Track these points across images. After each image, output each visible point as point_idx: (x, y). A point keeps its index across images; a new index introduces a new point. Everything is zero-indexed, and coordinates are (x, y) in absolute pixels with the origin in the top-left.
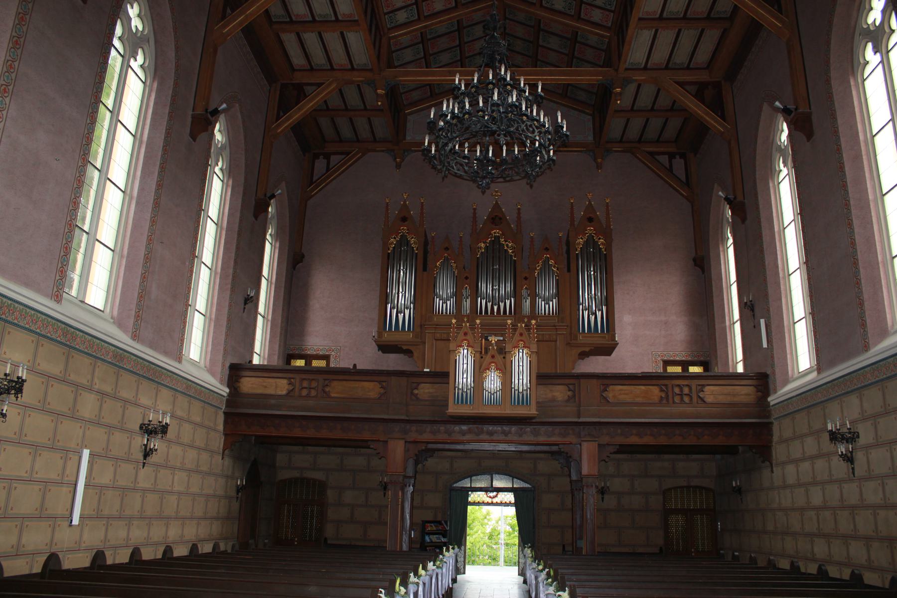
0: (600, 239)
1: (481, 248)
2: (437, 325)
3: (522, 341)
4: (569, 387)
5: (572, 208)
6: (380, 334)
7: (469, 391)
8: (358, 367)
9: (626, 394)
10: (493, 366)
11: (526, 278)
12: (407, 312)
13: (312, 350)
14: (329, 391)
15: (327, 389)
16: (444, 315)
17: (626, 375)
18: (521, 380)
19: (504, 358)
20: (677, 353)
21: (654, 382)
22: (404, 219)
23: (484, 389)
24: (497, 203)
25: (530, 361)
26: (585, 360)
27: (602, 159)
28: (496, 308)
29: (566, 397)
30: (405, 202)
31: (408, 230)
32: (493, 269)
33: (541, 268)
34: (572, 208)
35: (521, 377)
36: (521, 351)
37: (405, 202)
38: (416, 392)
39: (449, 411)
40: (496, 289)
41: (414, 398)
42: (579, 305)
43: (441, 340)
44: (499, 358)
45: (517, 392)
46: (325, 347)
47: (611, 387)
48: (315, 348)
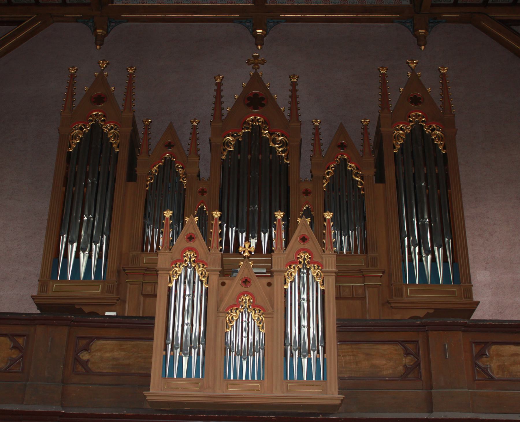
0: (433, 130)
1: (228, 144)
2: (146, 270)
6: (43, 286)
11: (307, 193)
18: (306, 329)
22: (99, 100)
25: (323, 292)
27: (426, 30)
31: (104, 116)
32: (248, 211)
35: (304, 323)
38: (85, 356)
41: (80, 369)
44: (259, 285)
47: (494, 347)
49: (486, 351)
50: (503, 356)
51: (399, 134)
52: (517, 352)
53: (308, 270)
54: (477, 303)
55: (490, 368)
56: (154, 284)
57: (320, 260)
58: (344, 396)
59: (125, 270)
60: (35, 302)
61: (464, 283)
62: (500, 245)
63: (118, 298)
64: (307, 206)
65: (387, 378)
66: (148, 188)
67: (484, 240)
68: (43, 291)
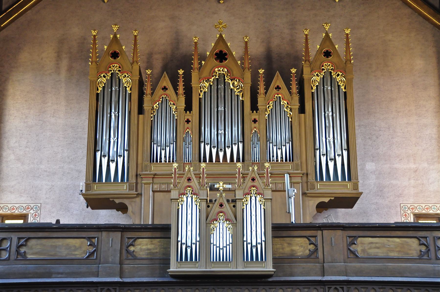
3: (221, 212)
4: (309, 240)
5: (307, 39)
6: (88, 187)
7: (194, 247)
8: (61, 222)
9: (378, 248)
10: (221, 217)
12: (120, 160)
13: (6, 209)
14: (25, 252)
15: (22, 250)
16: (163, 164)
17: (377, 225)
19: (234, 206)
20: (430, 205)
21: (410, 233)
23: (211, 243)
24: (221, 36)
26: (322, 213)
28: (221, 154)
29: (307, 252)
30: (115, 36)
33: (272, 109)
34: (307, 39)
36: (253, 198)
37: (115, 36)
38: (132, 249)
39: (171, 270)
40: (221, 134)
42: (315, 149)
43: (160, 191)
45: (249, 246)
46: (22, 205)
47: (359, 239)
48: (10, 206)
49: (355, 241)
50: (365, 244)
51: (315, 80)
52: (372, 242)
53: (256, 197)
54: (361, 193)
55: (357, 251)
56: (159, 184)
57: (262, 192)
58: (275, 270)
59: (140, 175)
60: (83, 197)
61: (353, 180)
62: (383, 145)
63: (137, 194)
64: (255, 129)
65: (300, 257)
66: (152, 119)
67: (372, 142)
68: (88, 190)
